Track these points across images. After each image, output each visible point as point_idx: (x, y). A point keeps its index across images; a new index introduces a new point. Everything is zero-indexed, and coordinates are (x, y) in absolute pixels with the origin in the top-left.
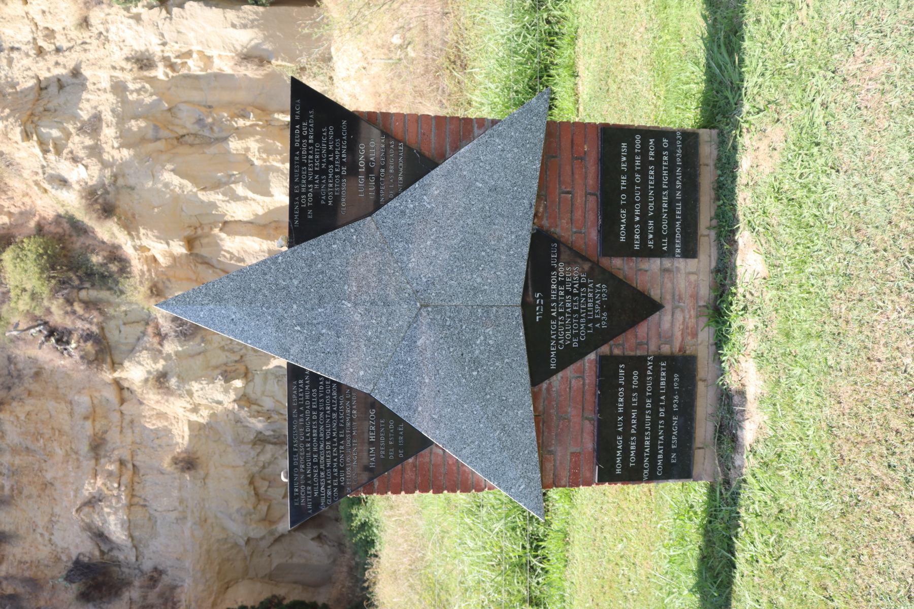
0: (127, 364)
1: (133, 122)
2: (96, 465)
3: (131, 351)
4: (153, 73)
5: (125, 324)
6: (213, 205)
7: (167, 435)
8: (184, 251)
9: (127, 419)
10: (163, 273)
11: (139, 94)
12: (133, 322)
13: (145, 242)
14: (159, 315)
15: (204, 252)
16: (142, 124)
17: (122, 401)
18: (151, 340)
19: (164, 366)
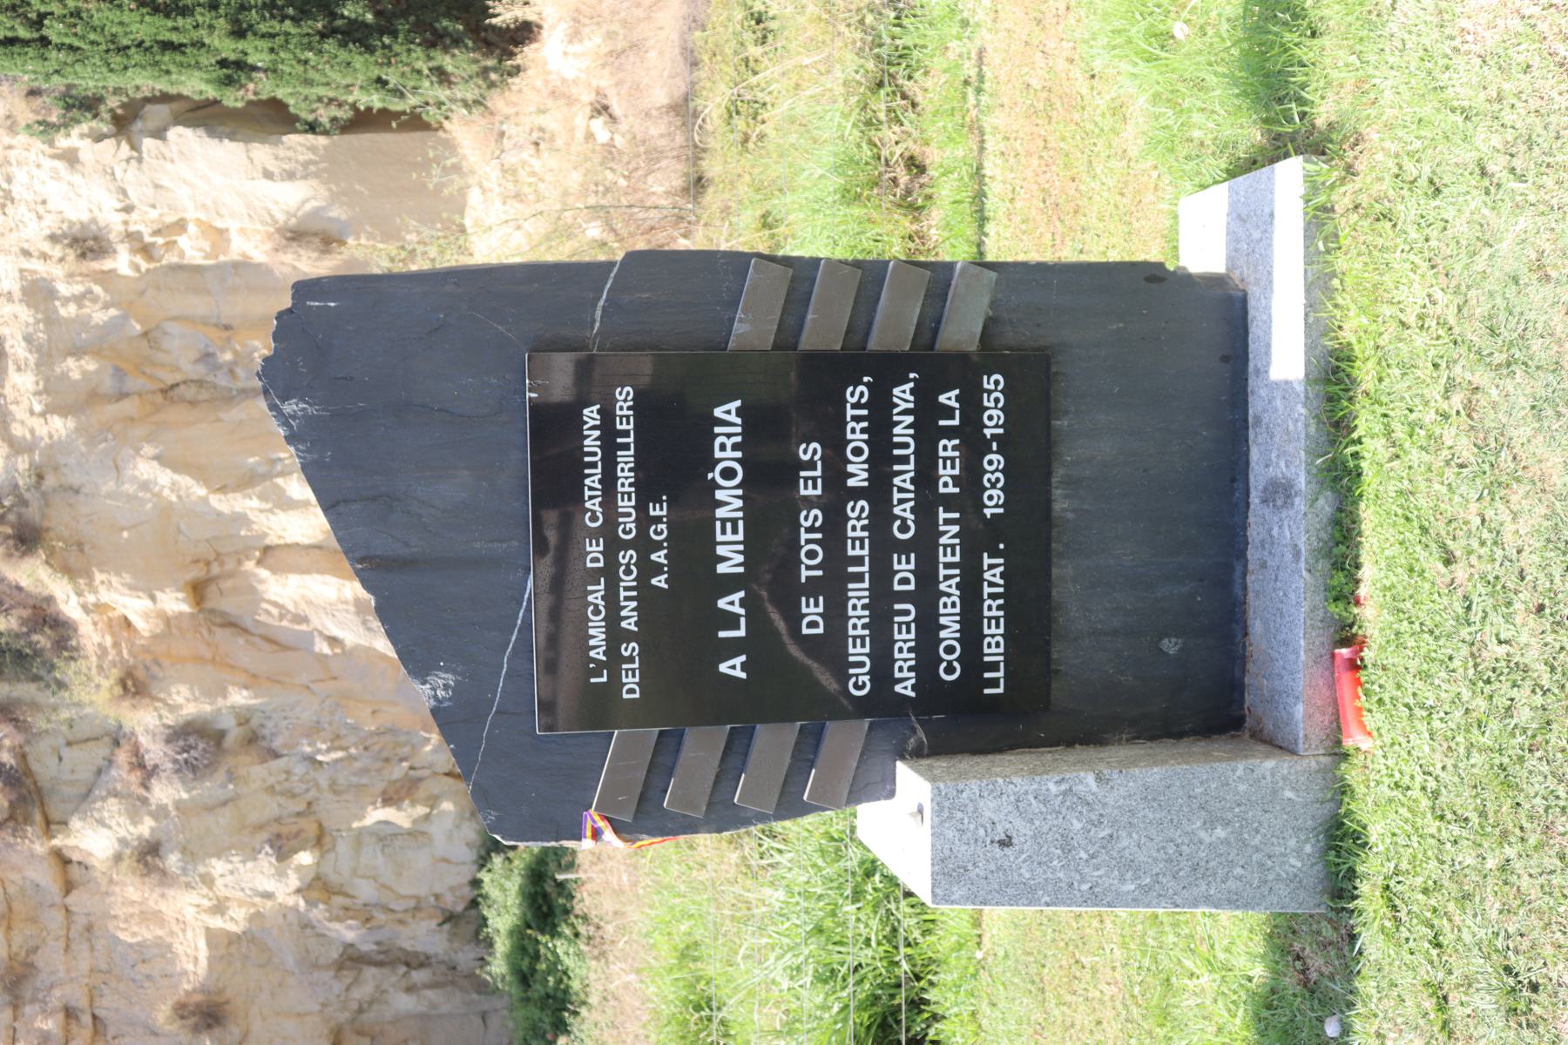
0: (76, 823)
1: (71, 362)
2: (15, 1019)
3: (85, 797)
4: (107, 264)
5: (69, 744)
6: (242, 519)
7: (163, 956)
8: (185, 608)
9: (81, 921)
10: (146, 649)
11: (80, 306)
12: (87, 740)
13: (105, 596)
14: (139, 730)
15: (229, 605)
16: (91, 365)
17: (69, 887)
18: (122, 774)
19: (152, 829)
